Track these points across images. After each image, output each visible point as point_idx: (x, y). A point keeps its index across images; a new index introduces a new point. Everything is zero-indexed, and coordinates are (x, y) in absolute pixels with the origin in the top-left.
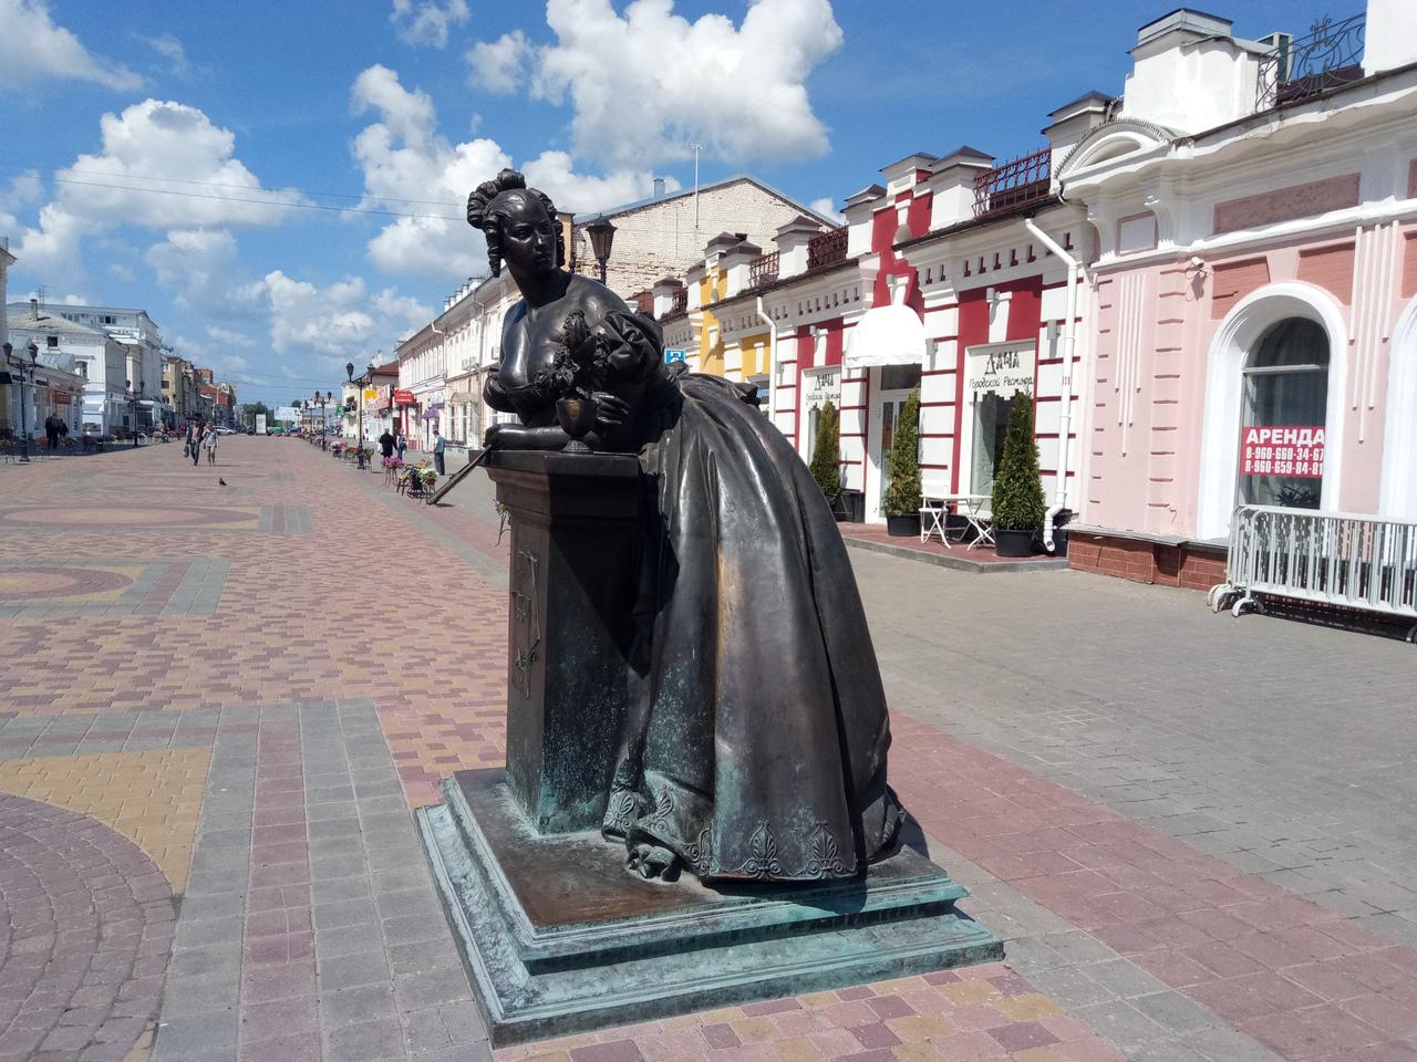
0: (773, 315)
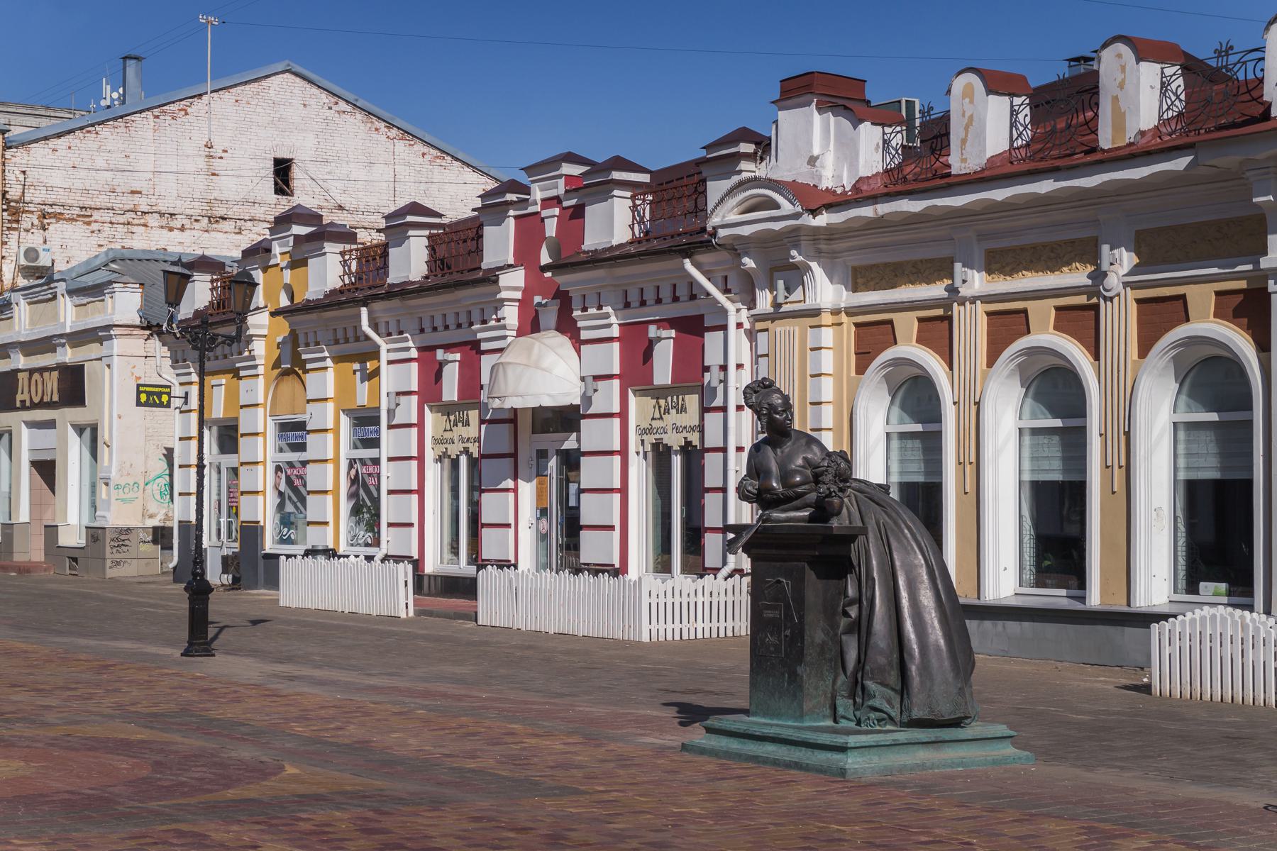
0: (382, 329)
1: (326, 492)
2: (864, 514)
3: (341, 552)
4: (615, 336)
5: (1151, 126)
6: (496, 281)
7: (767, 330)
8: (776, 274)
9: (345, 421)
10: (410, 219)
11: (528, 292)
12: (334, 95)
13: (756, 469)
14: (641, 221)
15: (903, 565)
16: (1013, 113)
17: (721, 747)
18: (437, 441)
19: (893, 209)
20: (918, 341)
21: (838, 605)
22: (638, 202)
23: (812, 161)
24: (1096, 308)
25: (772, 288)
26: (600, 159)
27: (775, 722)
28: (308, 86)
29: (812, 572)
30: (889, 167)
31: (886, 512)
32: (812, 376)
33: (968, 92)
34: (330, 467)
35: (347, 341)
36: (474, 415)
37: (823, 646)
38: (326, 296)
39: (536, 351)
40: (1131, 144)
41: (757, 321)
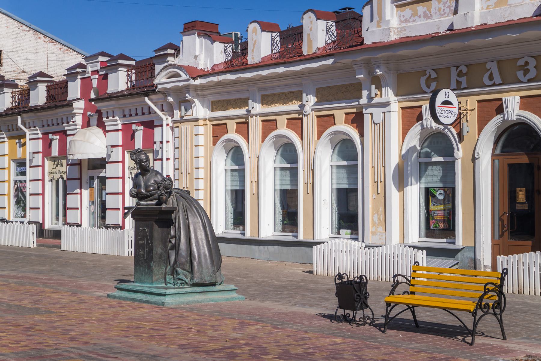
0: (27, 125)
1: (5, 195)
2: (178, 202)
3: (11, 220)
4: (120, 129)
5: (322, 46)
6: (72, 106)
7: (178, 127)
8: (181, 104)
9: (13, 164)
10: (38, 78)
11: (86, 110)
12: (21, 23)
13: (136, 185)
14: (131, 81)
15: (192, 222)
16: (273, 39)
17: (122, 295)
18: (50, 173)
19: (225, 78)
20: (236, 132)
21: (168, 239)
22: (129, 73)
23: (196, 57)
24: (301, 119)
25: (180, 110)
26: (115, 54)
27: (141, 285)
28: (9, 19)
29: (156, 225)
30: (226, 60)
31: (187, 202)
32: (195, 146)
33: (255, 31)
34: (6, 184)
35: (13, 130)
36: (64, 162)
37: (161, 255)
38: (5, 111)
39: (87, 135)
40: (314, 53)
41: (174, 123)
